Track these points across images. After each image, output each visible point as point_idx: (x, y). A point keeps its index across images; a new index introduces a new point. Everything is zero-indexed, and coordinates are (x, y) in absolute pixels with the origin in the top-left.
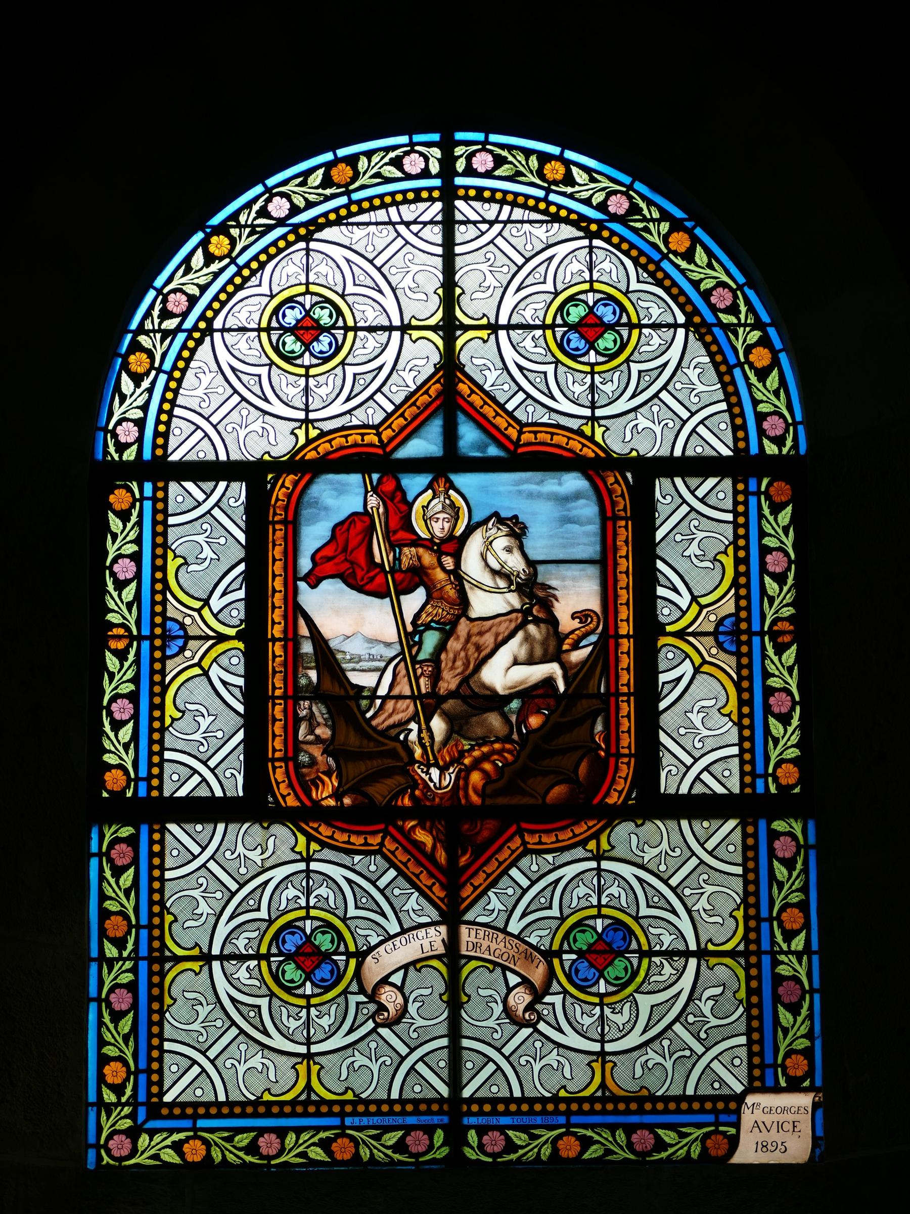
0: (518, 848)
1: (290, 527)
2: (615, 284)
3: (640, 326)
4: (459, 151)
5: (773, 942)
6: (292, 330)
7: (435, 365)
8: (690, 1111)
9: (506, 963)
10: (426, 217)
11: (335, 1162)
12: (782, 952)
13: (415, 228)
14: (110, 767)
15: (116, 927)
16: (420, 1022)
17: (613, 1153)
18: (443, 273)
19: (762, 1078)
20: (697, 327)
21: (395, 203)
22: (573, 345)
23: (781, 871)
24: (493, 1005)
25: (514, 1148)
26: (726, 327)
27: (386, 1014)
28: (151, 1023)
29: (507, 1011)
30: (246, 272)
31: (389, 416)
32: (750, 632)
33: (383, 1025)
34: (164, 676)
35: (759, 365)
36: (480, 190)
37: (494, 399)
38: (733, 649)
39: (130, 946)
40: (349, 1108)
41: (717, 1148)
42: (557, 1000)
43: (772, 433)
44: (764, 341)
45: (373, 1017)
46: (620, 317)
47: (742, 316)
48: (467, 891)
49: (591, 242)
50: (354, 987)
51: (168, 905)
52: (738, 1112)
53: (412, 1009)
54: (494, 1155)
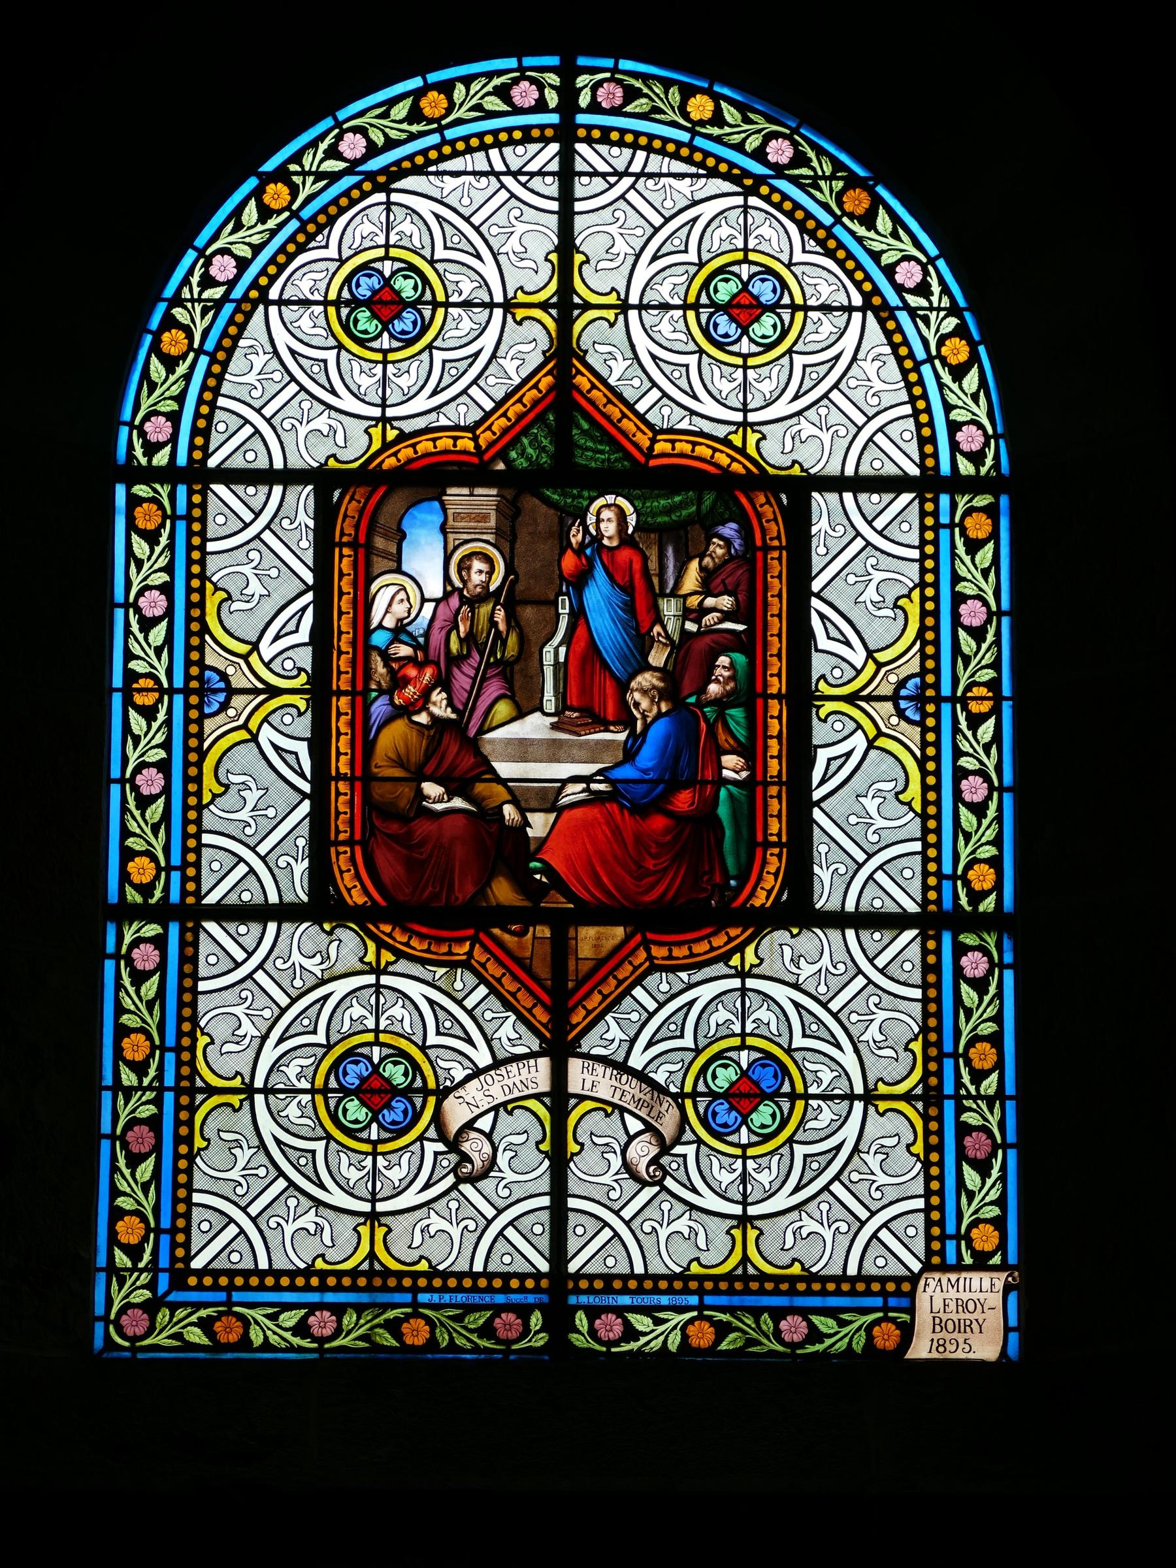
1: (361, 551)
2: (777, 255)
3: (806, 308)
4: (582, 81)
5: (959, 1084)
6: (404, 305)
7: (544, 353)
9: (625, 1105)
10: (533, 167)
11: (405, 1348)
12: (969, 1096)
13: (523, 179)
15: (136, 1047)
16: (510, 1176)
17: (757, 1343)
18: (558, 237)
19: (942, 1253)
20: (876, 312)
21: (498, 144)
22: (721, 331)
26: (912, 312)
28: (176, 1171)
29: (627, 1166)
30: (311, 228)
34: (202, 741)
36: (606, 130)
37: (620, 397)
39: (152, 1072)
40: (422, 1282)
41: (887, 1337)
42: (690, 1150)
44: (961, 331)
45: (454, 1170)
46: (781, 297)
49: (746, 200)
50: (432, 1133)
51: (202, 1024)
52: (912, 1295)
53: (502, 1160)
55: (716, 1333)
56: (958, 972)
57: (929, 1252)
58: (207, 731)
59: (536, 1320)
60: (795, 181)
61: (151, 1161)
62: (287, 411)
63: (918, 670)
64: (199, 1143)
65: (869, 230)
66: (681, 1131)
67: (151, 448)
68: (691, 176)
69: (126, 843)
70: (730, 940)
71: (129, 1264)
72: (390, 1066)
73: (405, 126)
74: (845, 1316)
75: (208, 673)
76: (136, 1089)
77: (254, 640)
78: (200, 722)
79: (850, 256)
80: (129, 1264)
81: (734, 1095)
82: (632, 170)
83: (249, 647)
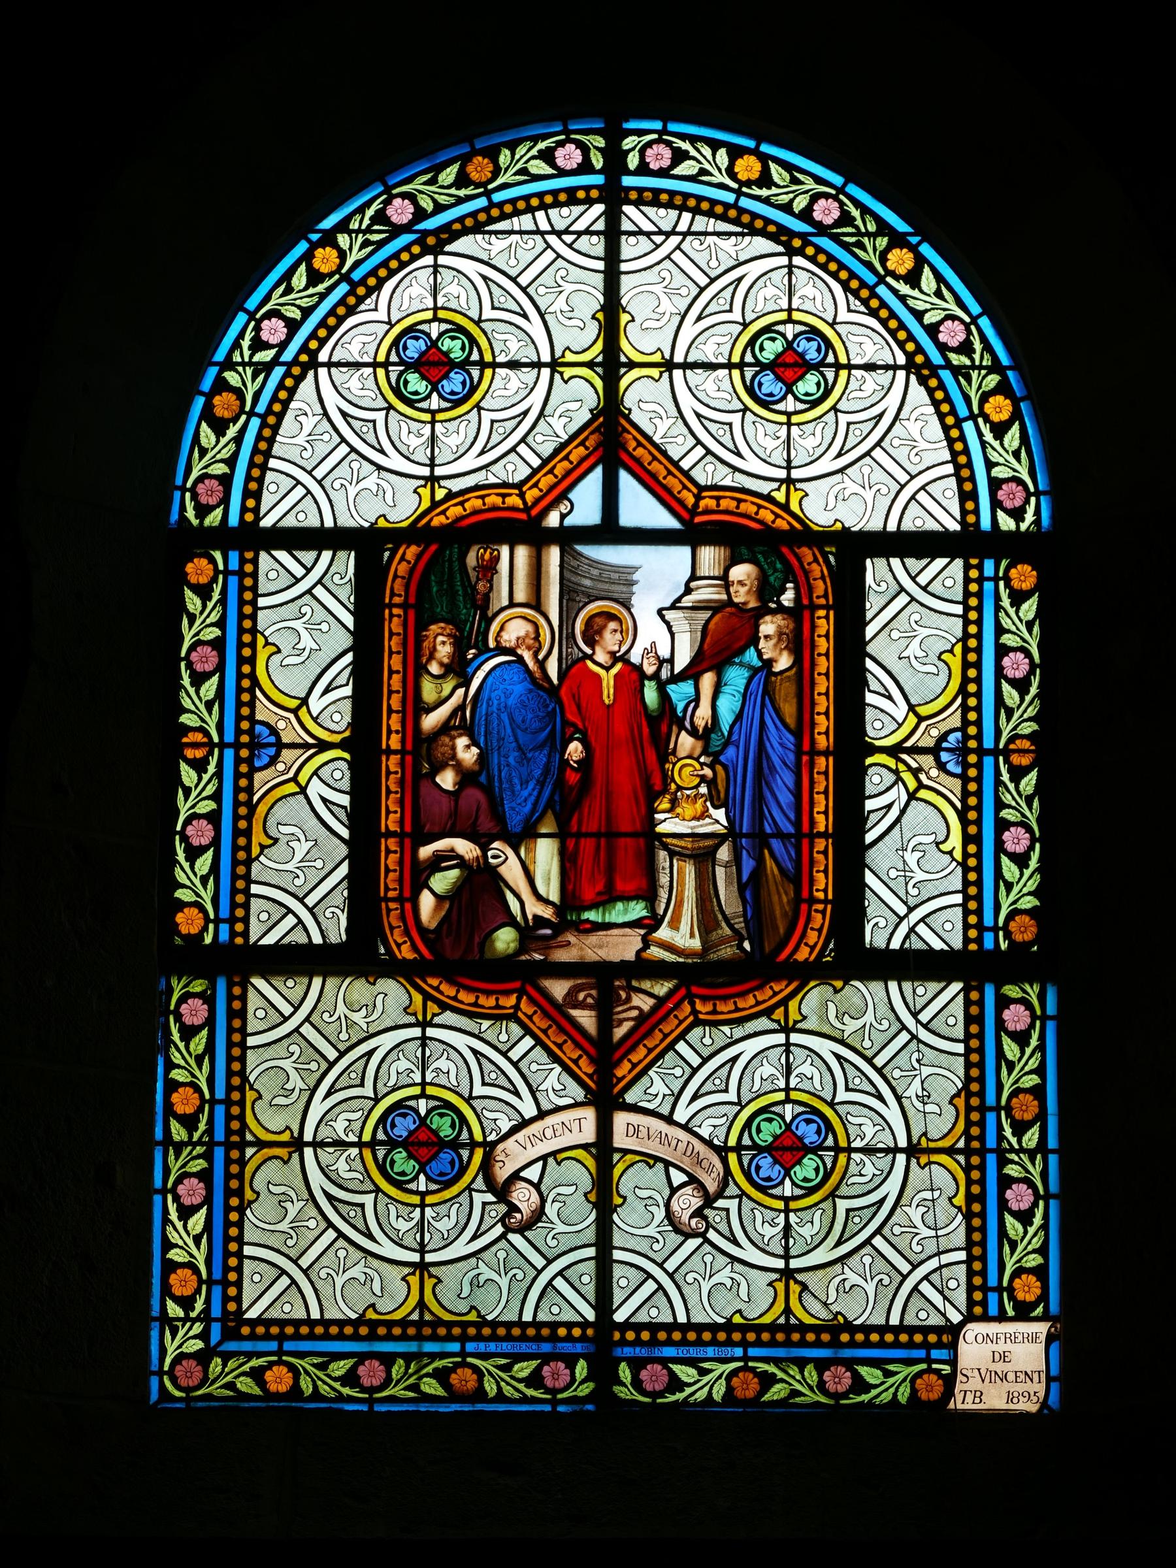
0: (686, 1018)
3: (850, 367)
5: (1001, 1137)
6: (452, 365)
7: (591, 411)
8: (896, 1344)
10: (580, 226)
11: (268, 1395)
13: (569, 238)
14: (181, 905)
19: (984, 1303)
21: (544, 207)
23: (1011, 1049)
24: (654, 1209)
25: (864, 1387)
26: (957, 371)
27: (518, 1216)
28: (228, 1224)
31: (535, 471)
32: (237, 746)
33: (514, 1231)
35: (996, 418)
38: (958, 770)
39: (202, 1126)
41: (931, 1390)
42: (733, 1205)
43: (1008, 504)
44: (1002, 388)
45: (502, 1220)
47: (977, 357)
48: (623, 1070)
49: (790, 260)
50: (480, 1183)
53: (551, 1210)
54: (655, 1395)
55: (760, 1383)
56: (1000, 1024)
57: (971, 1303)
58: (256, 785)
59: (581, 1369)
60: (836, 238)
61: (215, 679)
62: (324, 1261)
63: (958, 724)
64: (249, 1195)
65: (913, 288)
66: (724, 1184)
67: (203, 511)
68: (736, 234)
69: (168, 1256)
70: (775, 994)
71: (181, 1314)
72: (436, 1118)
73: (453, 191)
74: (891, 1367)
75: (258, 728)
76: (186, 1144)
77: (303, 695)
78: (250, 777)
79: (893, 315)
80: (181, 1314)
81: (777, 1149)
82: (678, 229)
83: (918, 795)
